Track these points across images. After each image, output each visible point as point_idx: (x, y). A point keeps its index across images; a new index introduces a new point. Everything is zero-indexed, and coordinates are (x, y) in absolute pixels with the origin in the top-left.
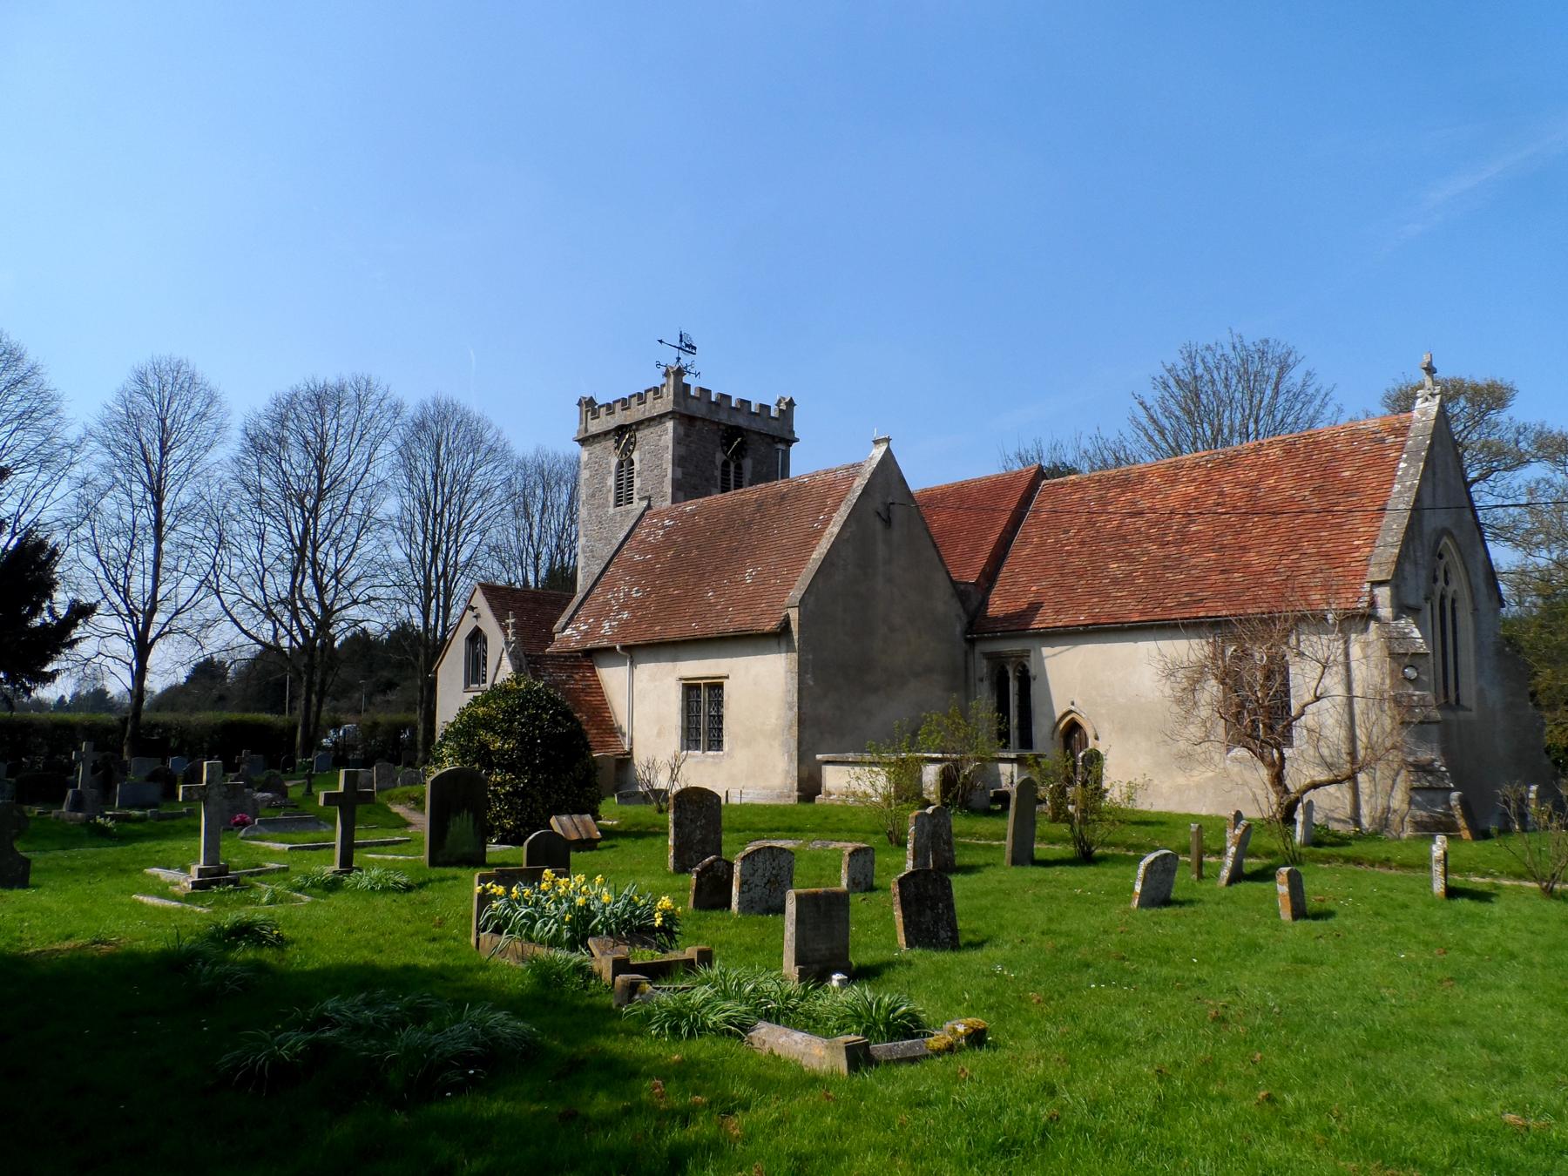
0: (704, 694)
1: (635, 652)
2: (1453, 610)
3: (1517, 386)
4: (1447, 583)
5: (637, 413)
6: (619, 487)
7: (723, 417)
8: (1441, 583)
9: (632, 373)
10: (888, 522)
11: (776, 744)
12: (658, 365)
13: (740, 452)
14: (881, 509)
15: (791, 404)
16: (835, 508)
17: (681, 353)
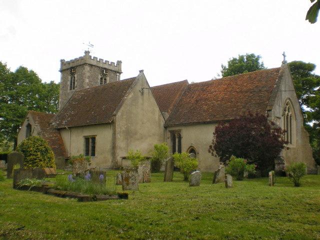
0: (91, 140)
1: (75, 127)
2: (291, 119)
4: (289, 112)
7: (101, 65)
10: (142, 94)
14: (140, 89)
17: (90, 47)
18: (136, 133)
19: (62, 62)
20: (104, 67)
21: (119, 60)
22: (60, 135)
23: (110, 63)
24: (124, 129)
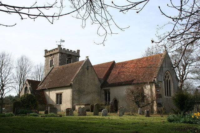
0: (59, 96)
1: (50, 89)
4: (168, 78)
5: (54, 52)
6: (51, 64)
7: (68, 53)
8: (167, 78)
9: (52, 46)
10: (88, 69)
11: (69, 103)
12: (57, 44)
13: (70, 58)
14: (86, 67)
15: (79, 51)
16: (79, 67)
19: (46, 51)
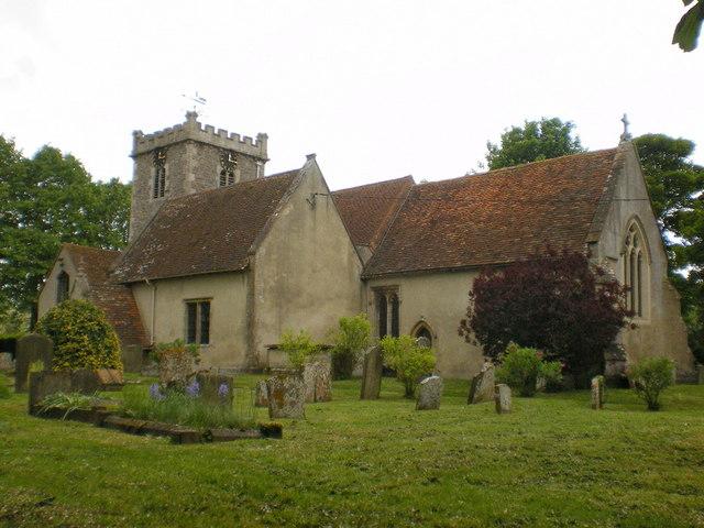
0: (199, 309)
1: (164, 279)
2: (639, 262)
3: (132, 132)
4: (635, 245)
7: (222, 144)
10: (313, 206)
14: (309, 196)
15: (311, 157)
17: (197, 104)
18: (299, 294)
19: (137, 136)
20: (229, 147)
21: (263, 132)
22: (133, 298)
23: (242, 140)
24: (272, 283)
